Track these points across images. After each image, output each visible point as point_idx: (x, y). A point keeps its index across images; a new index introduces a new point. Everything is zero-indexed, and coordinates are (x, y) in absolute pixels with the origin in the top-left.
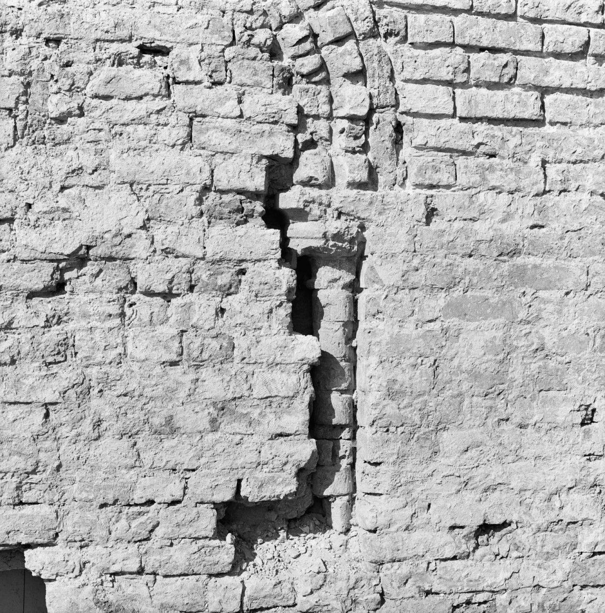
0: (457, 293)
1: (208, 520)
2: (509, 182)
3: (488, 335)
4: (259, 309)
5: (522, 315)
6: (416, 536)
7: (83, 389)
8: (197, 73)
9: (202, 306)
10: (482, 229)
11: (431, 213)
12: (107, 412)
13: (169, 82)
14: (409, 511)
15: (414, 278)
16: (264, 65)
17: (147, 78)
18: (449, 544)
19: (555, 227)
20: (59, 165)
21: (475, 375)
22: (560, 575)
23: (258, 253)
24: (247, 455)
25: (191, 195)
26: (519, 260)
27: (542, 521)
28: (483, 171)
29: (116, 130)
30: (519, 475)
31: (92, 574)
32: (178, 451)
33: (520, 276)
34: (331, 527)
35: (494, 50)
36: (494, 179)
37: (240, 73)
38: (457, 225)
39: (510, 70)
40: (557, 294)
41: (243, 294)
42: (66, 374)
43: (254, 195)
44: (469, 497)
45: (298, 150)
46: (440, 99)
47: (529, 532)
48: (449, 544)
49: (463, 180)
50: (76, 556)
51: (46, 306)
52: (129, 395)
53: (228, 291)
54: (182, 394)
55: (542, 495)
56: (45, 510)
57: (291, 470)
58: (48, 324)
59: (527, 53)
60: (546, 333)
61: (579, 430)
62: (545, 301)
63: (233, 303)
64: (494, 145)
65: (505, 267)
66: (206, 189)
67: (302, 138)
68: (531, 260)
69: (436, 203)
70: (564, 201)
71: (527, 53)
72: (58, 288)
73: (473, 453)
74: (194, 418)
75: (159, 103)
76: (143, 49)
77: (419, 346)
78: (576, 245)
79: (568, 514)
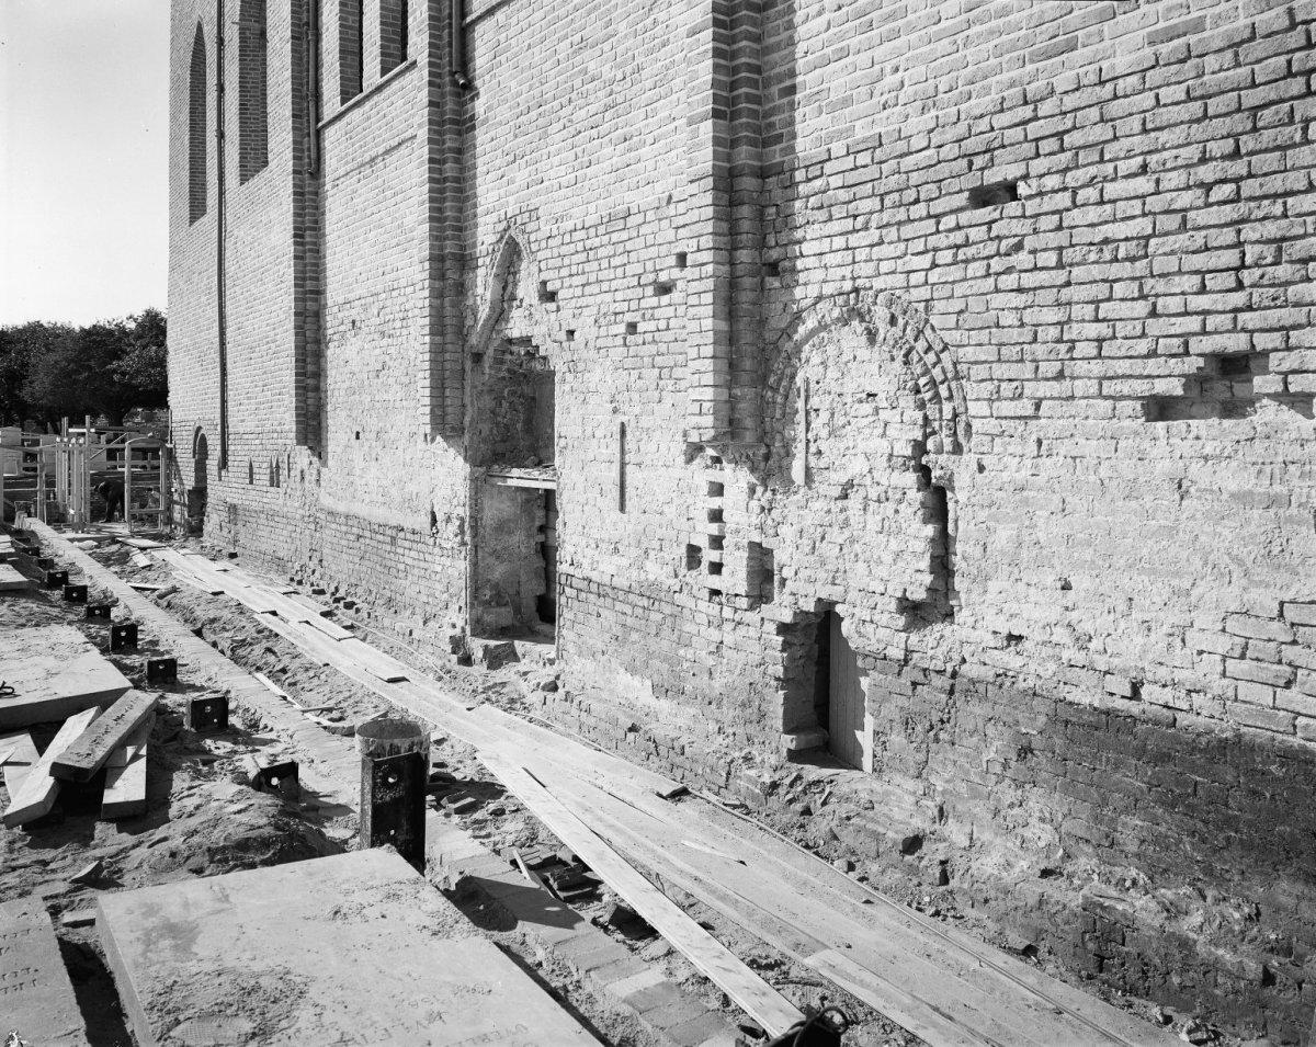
0: (994, 509)
1: (893, 606)
2: (1019, 451)
3: (1009, 533)
4: (911, 510)
5: (1027, 523)
6: (977, 632)
7: (853, 540)
8: (885, 404)
9: (890, 507)
10: (1005, 476)
11: (981, 468)
12: (859, 551)
13: (877, 410)
14: (973, 619)
15: (973, 500)
16: (911, 398)
17: (867, 408)
18: (991, 641)
19: (1043, 477)
20: (842, 446)
21: (1002, 552)
22: (1050, 673)
23: (909, 485)
24: (906, 578)
25: (885, 458)
26: (1025, 493)
27: (1039, 639)
28: (1005, 445)
29: (859, 431)
30: (1028, 611)
31: (856, 619)
32: (882, 571)
33: (1026, 501)
34: (842, 619)
35: (1010, 380)
36: (1011, 449)
37: (902, 403)
38: (993, 474)
39: (1019, 390)
40: (1046, 514)
41: (905, 504)
42: (847, 533)
43: (909, 458)
44: (1002, 618)
45: (926, 436)
46: (629, 245)
47: (1033, 644)
48: (991, 641)
49: (996, 450)
50: (851, 610)
51: (840, 504)
52: (303, 457)
53: (900, 501)
54: (883, 546)
55: (1040, 625)
56: (842, 588)
57: (923, 588)
58: (841, 511)
59: (1028, 380)
60: (1040, 534)
61: (1060, 592)
62: (1040, 517)
63: (902, 507)
64: (1012, 431)
65: (1018, 497)
66: (891, 455)
67: (928, 430)
68: (1032, 494)
69: (984, 463)
70: (1048, 461)
71: (1028, 380)
72: (846, 497)
73: (1003, 594)
74: (888, 558)
75: (871, 419)
76: (869, 395)
77: (976, 535)
78: (1057, 486)
79: (1055, 639)
